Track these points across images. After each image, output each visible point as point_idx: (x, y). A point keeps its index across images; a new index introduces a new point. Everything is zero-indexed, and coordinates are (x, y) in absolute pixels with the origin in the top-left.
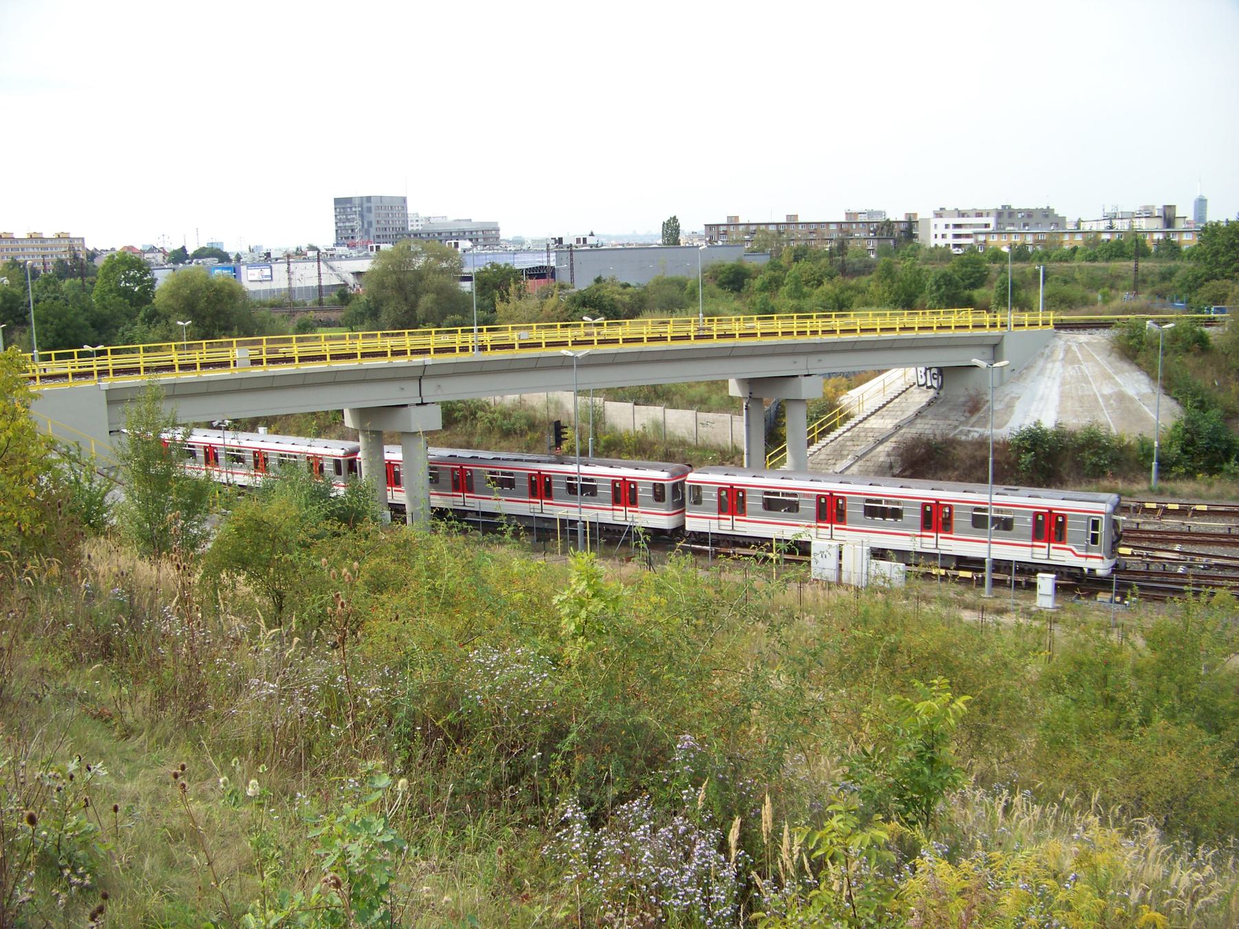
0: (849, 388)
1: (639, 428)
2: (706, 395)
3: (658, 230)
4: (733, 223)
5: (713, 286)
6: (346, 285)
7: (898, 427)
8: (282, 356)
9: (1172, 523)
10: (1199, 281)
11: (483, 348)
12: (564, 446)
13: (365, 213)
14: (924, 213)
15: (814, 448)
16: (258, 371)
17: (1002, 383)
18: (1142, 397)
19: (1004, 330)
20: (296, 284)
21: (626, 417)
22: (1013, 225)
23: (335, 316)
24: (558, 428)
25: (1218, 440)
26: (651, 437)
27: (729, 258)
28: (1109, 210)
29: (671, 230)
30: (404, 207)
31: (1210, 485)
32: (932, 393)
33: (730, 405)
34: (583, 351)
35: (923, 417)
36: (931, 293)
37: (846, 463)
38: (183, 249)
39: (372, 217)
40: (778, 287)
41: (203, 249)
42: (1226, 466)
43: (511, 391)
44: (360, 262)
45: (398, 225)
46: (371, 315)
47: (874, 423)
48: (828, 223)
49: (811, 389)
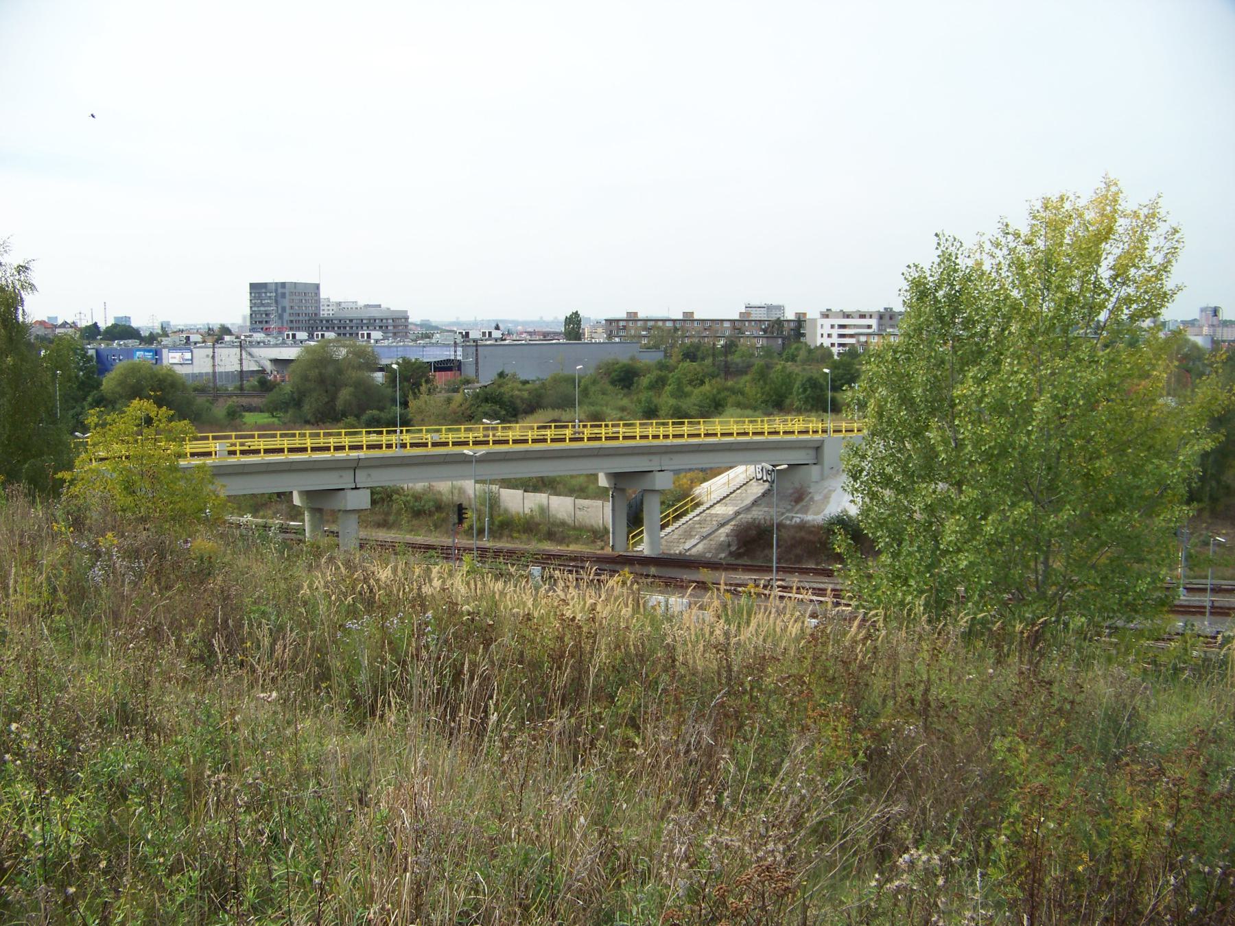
0: (705, 480)
1: (527, 511)
4: (632, 318)
7: (737, 513)
11: (404, 446)
12: (466, 525)
14: (812, 314)
15: (668, 530)
16: (233, 460)
17: (823, 479)
19: (825, 435)
20: (218, 369)
21: (516, 502)
23: (256, 401)
24: (461, 510)
26: (537, 519)
27: (622, 355)
29: (574, 322)
30: (317, 294)
32: (767, 485)
33: (601, 494)
34: (482, 450)
36: (798, 394)
37: (694, 541)
39: (286, 303)
40: (664, 385)
43: (422, 480)
44: (277, 350)
45: (311, 310)
47: (719, 510)
48: (722, 321)
49: (663, 482)
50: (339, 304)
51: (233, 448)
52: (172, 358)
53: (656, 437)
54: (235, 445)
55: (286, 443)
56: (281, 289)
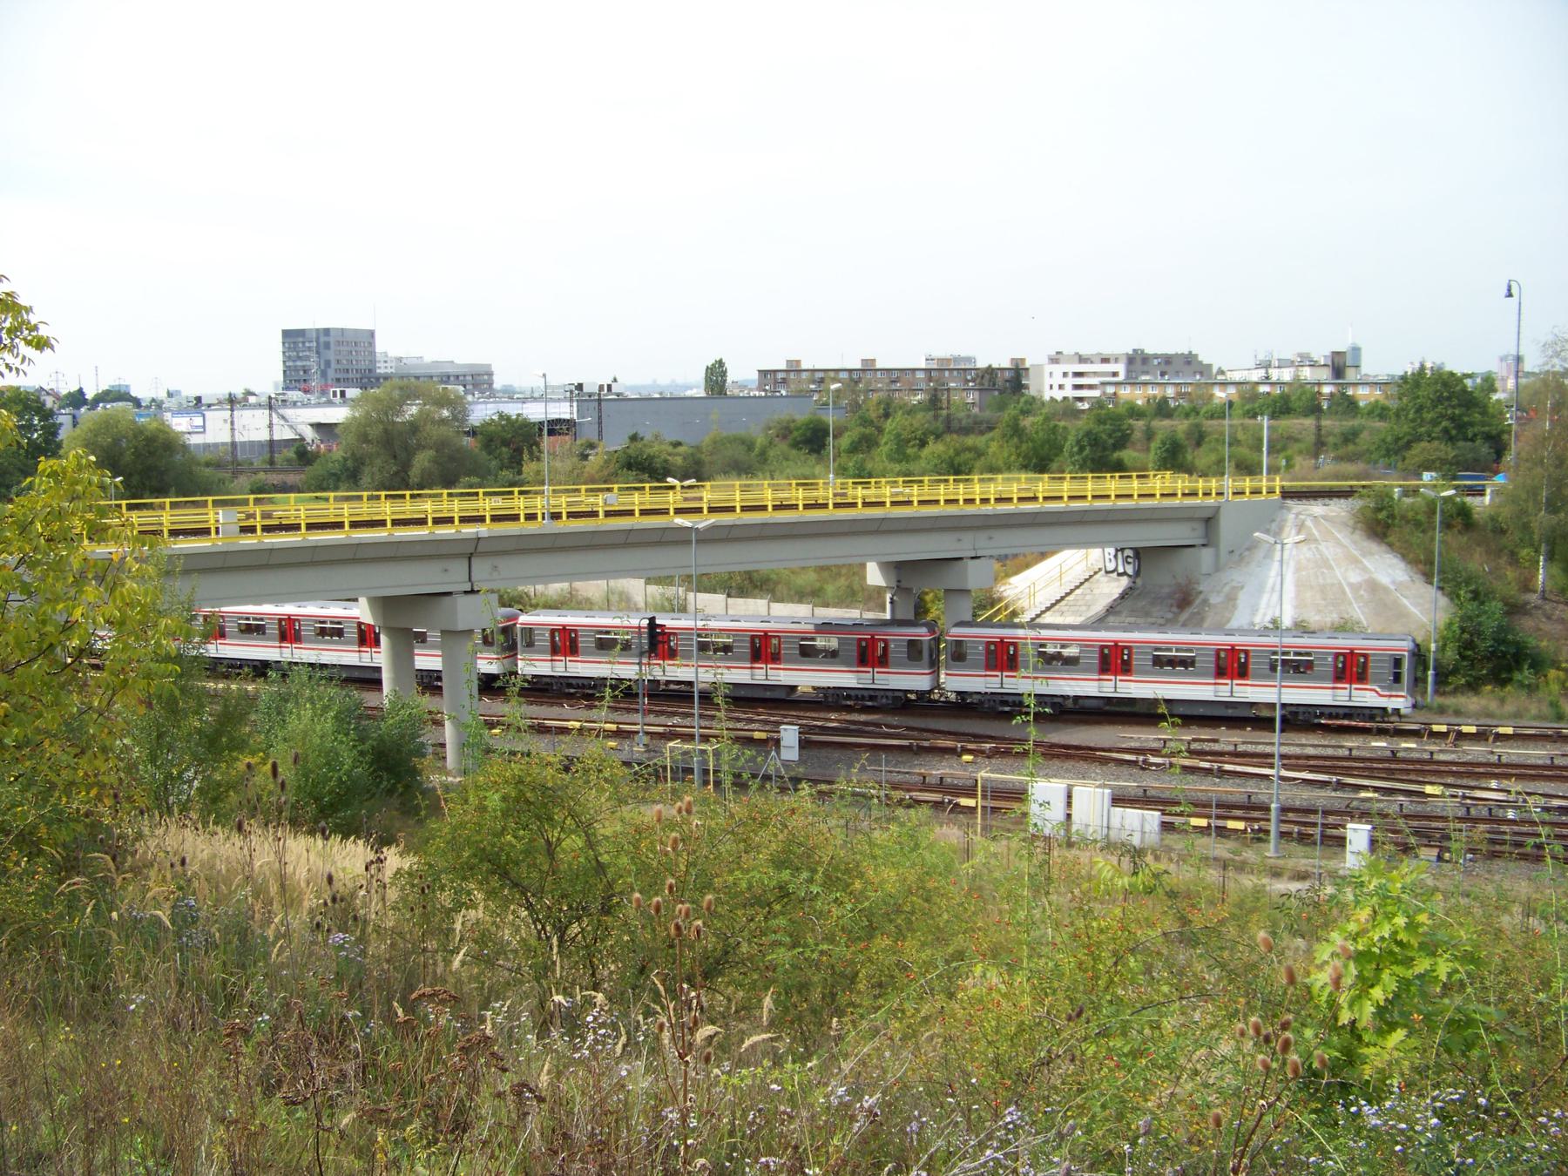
2: (818, 585)
3: (698, 377)
4: (794, 368)
5: (783, 446)
6: (303, 439)
8: (276, 522)
9: (1475, 751)
10: (1401, 443)
13: (322, 350)
16: (249, 541)
18: (1399, 586)
20: (239, 438)
22: (1147, 373)
23: (291, 478)
25: (1504, 642)
27: (801, 414)
28: (1261, 357)
29: (716, 376)
30: (372, 344)
31: (1502, 701)
35: (1118, 613)
36: (1072, 455)
38: (81, 391)
39: (331, 355)
41: (107, 393)
42: (1517, 676)
43: (559, 577)
45: (363, 366)
46: (348, 477)
50: (400, 359)
51: (251, 522)
52: (179, 424)
53: (985, 501)
54: (253, 516)
55: (347, 512)
56: (324, 339)
